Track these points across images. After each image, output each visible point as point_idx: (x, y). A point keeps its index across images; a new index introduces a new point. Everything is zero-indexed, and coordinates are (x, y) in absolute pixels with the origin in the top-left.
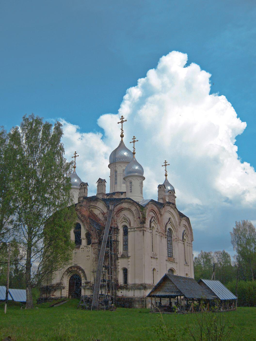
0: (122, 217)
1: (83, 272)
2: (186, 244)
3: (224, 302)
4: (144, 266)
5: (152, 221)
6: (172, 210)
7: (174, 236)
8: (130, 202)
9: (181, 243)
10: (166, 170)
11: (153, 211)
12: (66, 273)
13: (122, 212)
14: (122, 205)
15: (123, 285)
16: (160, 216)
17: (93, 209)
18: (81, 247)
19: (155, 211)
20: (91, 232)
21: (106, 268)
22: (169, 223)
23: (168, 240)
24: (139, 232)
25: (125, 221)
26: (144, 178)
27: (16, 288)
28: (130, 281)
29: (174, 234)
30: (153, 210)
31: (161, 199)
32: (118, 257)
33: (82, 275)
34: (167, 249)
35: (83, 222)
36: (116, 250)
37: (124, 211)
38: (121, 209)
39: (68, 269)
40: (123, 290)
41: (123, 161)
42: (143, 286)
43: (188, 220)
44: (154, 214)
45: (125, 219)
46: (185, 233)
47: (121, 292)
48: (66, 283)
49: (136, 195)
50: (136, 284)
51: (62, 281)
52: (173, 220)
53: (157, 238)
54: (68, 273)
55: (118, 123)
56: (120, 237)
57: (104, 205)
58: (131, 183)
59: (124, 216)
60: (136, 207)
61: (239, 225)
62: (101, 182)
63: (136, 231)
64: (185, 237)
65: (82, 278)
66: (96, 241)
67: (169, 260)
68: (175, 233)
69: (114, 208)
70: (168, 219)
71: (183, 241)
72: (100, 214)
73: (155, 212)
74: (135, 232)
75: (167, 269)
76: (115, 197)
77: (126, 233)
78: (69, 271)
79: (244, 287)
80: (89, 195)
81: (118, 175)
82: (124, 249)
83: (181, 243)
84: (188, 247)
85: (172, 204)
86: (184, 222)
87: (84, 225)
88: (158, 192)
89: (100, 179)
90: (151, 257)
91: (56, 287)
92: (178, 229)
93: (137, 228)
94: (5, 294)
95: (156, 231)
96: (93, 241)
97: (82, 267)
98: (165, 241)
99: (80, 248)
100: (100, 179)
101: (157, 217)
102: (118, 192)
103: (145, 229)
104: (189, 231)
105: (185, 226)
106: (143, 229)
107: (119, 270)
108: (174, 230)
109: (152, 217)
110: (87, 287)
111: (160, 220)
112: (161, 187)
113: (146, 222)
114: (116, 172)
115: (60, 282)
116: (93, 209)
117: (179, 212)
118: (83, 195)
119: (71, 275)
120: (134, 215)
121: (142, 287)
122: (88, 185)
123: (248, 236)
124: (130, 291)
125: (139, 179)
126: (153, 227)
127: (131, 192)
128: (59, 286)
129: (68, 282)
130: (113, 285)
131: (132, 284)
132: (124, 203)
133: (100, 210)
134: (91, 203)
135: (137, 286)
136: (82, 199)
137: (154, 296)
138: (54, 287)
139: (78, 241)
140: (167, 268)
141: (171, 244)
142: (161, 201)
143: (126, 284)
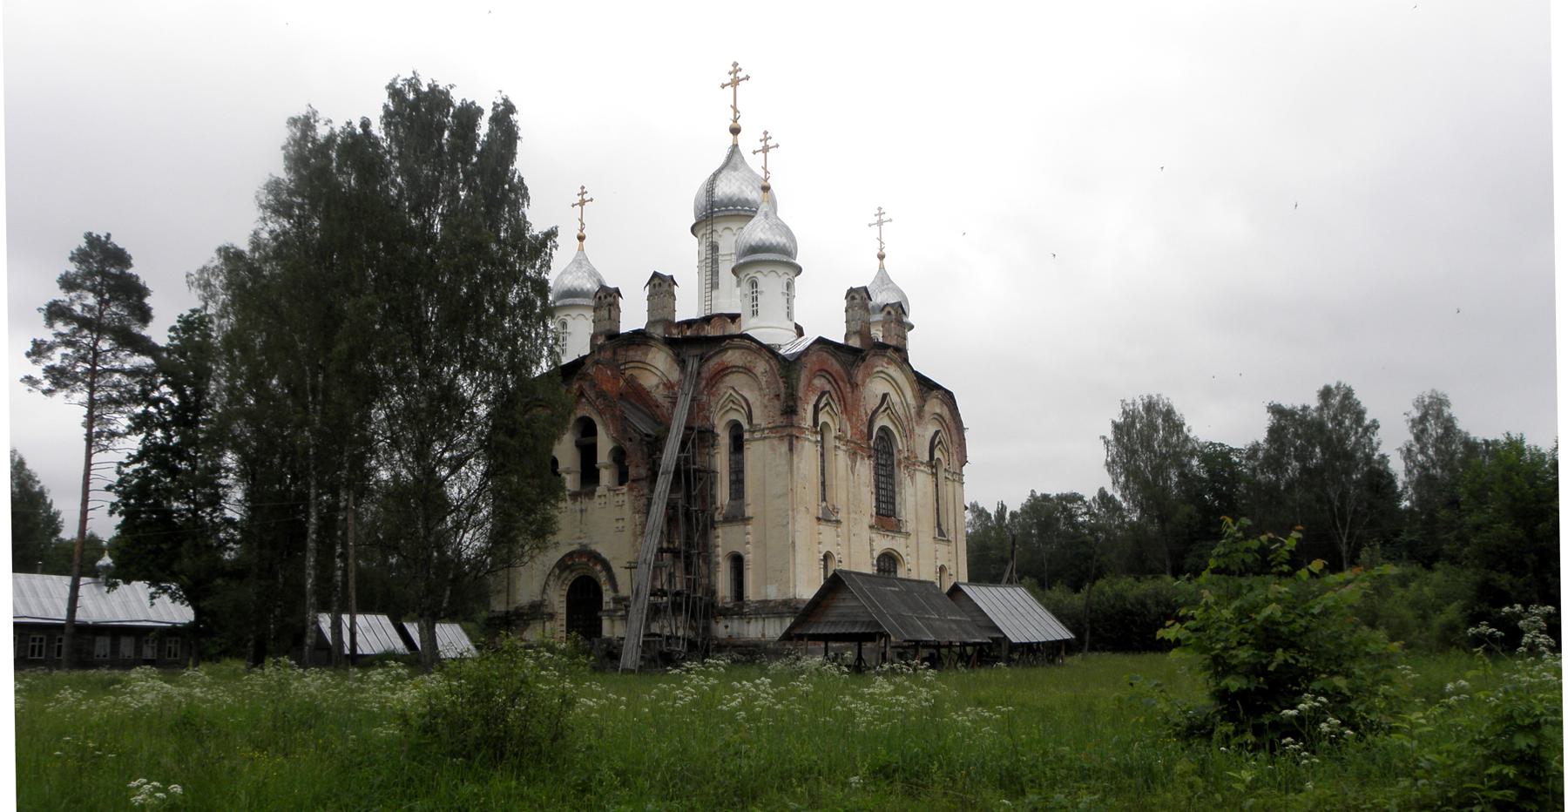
0: (727, 395)
1: (607, 566)
2: (941, 474)
3: (1030, 649)
4: (794, 547)
5: (821, 405)
6: (893, 371)
7: (899, 451)
8: (748, 348)
9: (922, 471)
10: (880, 240)
11: (823, 372)
12: (557, 571)
13: (728, 378)
14: (724, 358)
15: (730, 605)
16: (849, 390)
17: (636, 372)
18: (600, 490)
19: (834, 374)
20: (628, 444)
21: (675, 553)
22: (882, 409)
23: (878, 464)
24: (776, 442)
25: (735, 407)
26: (798, 270)
27: (45, 571)
28: (751, 593)
29: (900, 443)
30: (827, 371)
31: (855, 333)
32: (716, 519)
33: (603, 577)
34: (873, 490)
35: (601, 413)
36: (708, 497)
37: (731, 376)
38: (724, 371)
39: (562, 560)
40: (732, 619)
41: (736, 212)
42: (790, 607)
43: (948, 398)
44: (830, 382)
45: (733, 402)
46: (937, 440)
47: (727, 627)
48: (558, 601)
49: (770, 324)
50: (770, 601)
51: (545, 597)
52: (898, 400)
53: (840, 460)
54: (562, 571)
55: (723, 86)
56: (721, 460)
57: (669, 359)
58: (754, 284)
59: (731, 391)
60: (768, 361)
61: (1133, 412)
62: (661, 286)
63: (769, 437)
64: (937, 454)
65: (604, 588)
66: (643, 472)
67: (883, 527)
68: (902, 441)
69: (700, 366)
70: (880, 397)
71: (932, 467)
72: (657, 387)
73: (833, 377)
74: (767, 441)
75: (872, 554)
76: (711, 331)
77: (738, 444)
78: (563, 565)
79: (1129, 606)
80: (625, 328)
81: (720, 258)
82: (733, 496)
83: (922, 471)
84: (948, 483)
85: (899, 353)
86: (935, 406)
87: (606, 425)
88: (846, 311)
89: (655, 275)
90: (819, 519)
91: (527, 614)
92: (916, 428)
93: (771, 429)
94: (68, 589)
95: (836, 437)
96: (632, 472)
97: (605, 554)
98: (865, 469)
99: (597, 494)
100: (655, 275)
101: (841, 392)
102: (720, 316)
103: (795, 432)
104: (954, 432)
105: (939, 418)
106: (789, 430)
107: (720, 559)
108: (899, 432)
109: (823, 394)
110: (619, 614)
111: (849, 401)
112: (857, 296)
113: (800, 410)
114: (714, 248)
115: (539, 598)
116: (636, 372)
117: (917, 374)
118: (606, 326)
119: (572, 577)
120: (761, 389)
121: (785, 610)
122: (620, 295)
123: (1159, 447)
124: (753, 621)
125: (781, 271)
126: (825, 424)
127: (755, 313)
128: (537, 612)
129: (564, 599)
130: (694, 603)
131: (758, 602)
132: (730, 352)
133: (659, 374)
134: (631, 353)
135: (772, 607)
136: (600, 341)
137: (800, 637)
138: (523, 614)
139: (589, 474)
140: (872, 550)
141: (891, 476)
142: (855, 342)
143: (740, 603)
